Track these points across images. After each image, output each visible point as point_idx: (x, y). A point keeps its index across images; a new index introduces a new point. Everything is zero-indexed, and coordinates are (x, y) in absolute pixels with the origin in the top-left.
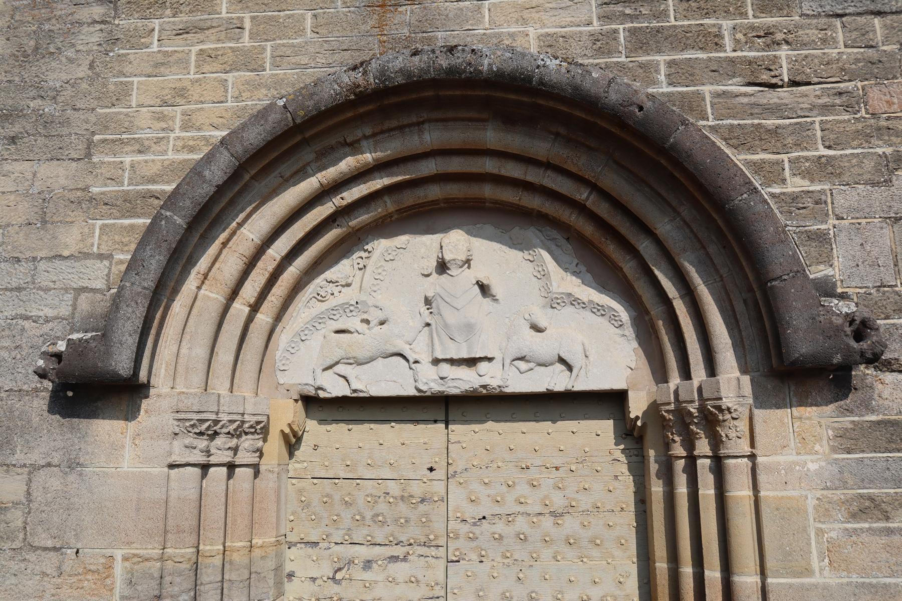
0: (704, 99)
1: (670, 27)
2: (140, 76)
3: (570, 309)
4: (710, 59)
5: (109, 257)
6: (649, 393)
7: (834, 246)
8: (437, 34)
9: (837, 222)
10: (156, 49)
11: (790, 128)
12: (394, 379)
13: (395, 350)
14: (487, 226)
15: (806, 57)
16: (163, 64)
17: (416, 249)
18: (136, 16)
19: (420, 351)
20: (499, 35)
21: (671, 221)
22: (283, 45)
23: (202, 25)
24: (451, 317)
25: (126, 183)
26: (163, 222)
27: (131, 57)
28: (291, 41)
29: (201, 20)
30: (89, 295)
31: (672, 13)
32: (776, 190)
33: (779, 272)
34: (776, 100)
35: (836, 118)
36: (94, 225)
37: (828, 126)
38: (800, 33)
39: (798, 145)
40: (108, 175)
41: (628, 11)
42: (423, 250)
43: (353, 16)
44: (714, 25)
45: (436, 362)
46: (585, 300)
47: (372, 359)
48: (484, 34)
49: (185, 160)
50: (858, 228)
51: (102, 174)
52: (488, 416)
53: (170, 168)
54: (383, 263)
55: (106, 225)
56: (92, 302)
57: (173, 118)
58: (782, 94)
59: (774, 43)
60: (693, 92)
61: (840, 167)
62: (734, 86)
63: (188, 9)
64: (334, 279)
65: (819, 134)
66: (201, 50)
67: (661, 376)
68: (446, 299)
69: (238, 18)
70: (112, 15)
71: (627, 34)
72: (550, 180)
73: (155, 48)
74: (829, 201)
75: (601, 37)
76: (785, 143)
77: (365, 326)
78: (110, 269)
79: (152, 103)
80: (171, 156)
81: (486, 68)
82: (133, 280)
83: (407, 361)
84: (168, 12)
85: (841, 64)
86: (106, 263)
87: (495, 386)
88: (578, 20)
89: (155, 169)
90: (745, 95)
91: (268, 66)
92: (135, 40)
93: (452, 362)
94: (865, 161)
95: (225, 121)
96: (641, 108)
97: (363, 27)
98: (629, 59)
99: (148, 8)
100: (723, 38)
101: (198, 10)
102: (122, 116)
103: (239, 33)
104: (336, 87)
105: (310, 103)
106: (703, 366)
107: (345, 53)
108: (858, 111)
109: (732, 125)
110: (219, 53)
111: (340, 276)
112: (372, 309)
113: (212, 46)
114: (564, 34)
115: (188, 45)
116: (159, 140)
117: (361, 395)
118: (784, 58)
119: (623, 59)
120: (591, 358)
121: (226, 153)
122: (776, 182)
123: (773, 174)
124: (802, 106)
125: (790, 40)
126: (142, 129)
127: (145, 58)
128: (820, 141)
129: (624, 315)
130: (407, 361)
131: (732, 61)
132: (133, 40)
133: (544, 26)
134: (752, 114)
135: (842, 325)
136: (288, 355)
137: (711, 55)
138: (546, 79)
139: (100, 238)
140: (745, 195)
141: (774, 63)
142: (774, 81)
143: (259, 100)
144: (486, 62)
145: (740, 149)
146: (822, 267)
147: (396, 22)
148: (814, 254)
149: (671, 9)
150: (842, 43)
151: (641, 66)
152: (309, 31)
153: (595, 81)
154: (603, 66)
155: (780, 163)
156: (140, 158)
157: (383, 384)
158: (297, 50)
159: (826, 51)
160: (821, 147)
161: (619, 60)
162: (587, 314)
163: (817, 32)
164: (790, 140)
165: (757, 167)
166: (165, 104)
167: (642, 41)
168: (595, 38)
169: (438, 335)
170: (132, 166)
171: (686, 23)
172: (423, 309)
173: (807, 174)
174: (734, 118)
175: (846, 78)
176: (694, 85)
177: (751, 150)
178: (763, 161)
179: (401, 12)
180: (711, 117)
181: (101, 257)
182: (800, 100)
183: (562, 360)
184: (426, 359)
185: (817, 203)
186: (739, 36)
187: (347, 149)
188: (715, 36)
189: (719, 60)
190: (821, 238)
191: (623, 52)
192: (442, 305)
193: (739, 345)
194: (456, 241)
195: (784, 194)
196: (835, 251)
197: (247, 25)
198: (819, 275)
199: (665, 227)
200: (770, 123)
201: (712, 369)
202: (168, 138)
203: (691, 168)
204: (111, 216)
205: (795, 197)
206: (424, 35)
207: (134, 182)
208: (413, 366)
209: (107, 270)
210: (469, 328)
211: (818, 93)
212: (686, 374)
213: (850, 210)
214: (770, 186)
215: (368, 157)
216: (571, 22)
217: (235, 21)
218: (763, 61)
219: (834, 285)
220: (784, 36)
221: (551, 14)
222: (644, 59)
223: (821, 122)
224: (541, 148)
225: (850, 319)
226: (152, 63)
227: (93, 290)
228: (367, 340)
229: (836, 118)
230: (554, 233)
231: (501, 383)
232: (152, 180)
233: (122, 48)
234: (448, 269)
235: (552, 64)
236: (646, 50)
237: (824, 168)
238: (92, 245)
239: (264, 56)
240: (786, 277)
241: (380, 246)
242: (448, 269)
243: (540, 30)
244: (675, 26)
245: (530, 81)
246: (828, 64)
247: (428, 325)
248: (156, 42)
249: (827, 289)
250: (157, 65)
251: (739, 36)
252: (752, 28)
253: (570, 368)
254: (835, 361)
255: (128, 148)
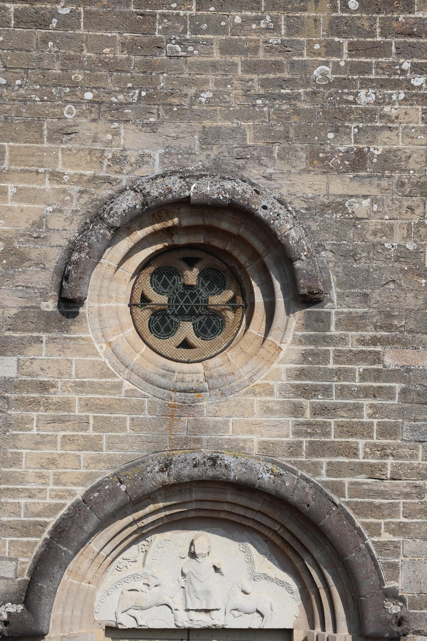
0: (344, 486)
1: (331, 442)
2: (27, 449)
3: (265, 581)
4: (350, 463)
5: (16, 560)
6: (305, 631)
7: (400, 571)
8: (202, 436)
9: (403, 558)
10: (36, 433)
11: (387, 506)
12: (163, 618)
13: (164, 603)
14: (219, 529)
15: (401, 464)
16: (41, 443)
17: (180, 538)
18: (22, 409)
19: (178, 603)
20: (237, 440)
21: (321, 551)
22: (114, 436)
23: (63, 419)
24: (198, 586)
25: (22, 515)
26: (63, 554)
27: (21, 436)
28: (118, 434)
29: (63, 415)
30: (5, 581)
31: (333, 433)
32: (376, 539)
33: (365, 593)
34: (382, 488)
35: (412, 501)
36: (5, 540)
37: (407, 506)
38: (400, 450)
39: (390, 515)
40: (12, 511)
41: (309, 430)
42: (181, 542)
43: (155, 421)
44: (355, 442)
45: (187, 610)
46: (273, 577)
47: (150, 607)
48: (229, 439)
49: (57, 504)
50: (413, 562)
51: (7, 510)
52: (213, 637)
53: (53, 509)
54: (157, 549)
55: (12, 541)
56: (7, 585)
57: (48, 477)
58: (387, 484)
59: (385, 455)
60: (339, 482)
61: (410, 529)
62: (361, 479)
63: (54, 407)
64: (128, 558)
65: (401, 509)
66: (64, 436)
67: (313, 627)
68: (195, 575)
69: (86, 416)
70: (6, 408)
71: (308, 444)
72: (259, 518)
73: (34, 431)
74: (401, 547)
75: (293, 445)
76: (384, 513)
77: (146, 587)
78: (16, 567)
79: (35, 467)
80: (49, 501)
81: (232, 477)
82: (48, 584)
83: (171, 608)
84: (42, 408)
85: (418, 470)
86: (14, 563)
87: (220, 625)
88: (282, 433)
89: (40, 508)
90: (367, 484)
91: (104, 448)
93: (197, 610)
94: (422, 526)
95: (79, 481)
96: (308, 506)
97: (160, 429)
98: (307, 459)
99: (29, 405)
100: (359, 450)
101: (61, 409)
102: (17, 474)
103: (87, 426)
104: (154, 483)
105: (140, 491)
106: (331, 625)
107: (150, 444)
108: (423, 498)
109: (357, 502)
110: (75, 438)
111: (131, 556)
112: (151, 578)
113: (71, 433)
114: (273, 442)
115: (55, 431)
116: (41, 491)
117: (144, 627)
118: (389, 465)
119: (304, 459)
120: (274, 611)
121: (95, 517)
123: (375, 530)
124: (396, 493)
125: (394, 454)
126: (30, 483)
127: (29, 438)
128: (401, 514)
129: (295, 587)
130: (171, 608)
131: (361, 464)
132: (21, 425)
133: (262, 436)
134: (368, 496)
135: (391, 620)
136: (100, 604)
137: (351, 460)
138: (263, 486)
139: (9, 548)
140: (354, 554)
141: (384, 467)
142: (383, 477)
143: (100, 469)
144: (232, 474)
145: (360, 515)
146: (393, 582)
147: (180, 427)
148: (390, 575)
149: (333, 430)
150: (420, 458)
151: (313, 464)
152: (128, 428)
153: (287, 489)
154: (293, 462)
155: (379, 525)
156: (30, 500)
157: (156, 622)
158: (122, 440)
159: (412, 462)
160: (401, 517)
161: (302, 459)
162: (274, 584)
163: (408, 450)
164: (386, 512)
165: (368, 526)
166: (43, 467)
167: (316, 449)
168: (290, 445)
169: (189, 595)
170: (26, 506)
171: (340, 440)
172: (180, 577)
173: (393, 532)
174: (359, 497)
175: (420, 478)
176: (340, 477)
177: (366, 516)
178: (371, 523)
179: (182, 421)
180: (347, 496)
181: (11, 559)
182: (395, 489)
183: (258, 611)
184: (181, 608)
185: (395, 547)
186: (368, 450)
187: (149, 500)
188: (354, 449)
189: (355, 464)
190: (394, 567)
191: (304, 455)
192: (193, 578)
193: (348, 618)
195: (379, 542)
196: (400, 574)
197: (91, 421)
198: (391, 586)
199: (317, 555)
200: (378, 501)
201: (335, 630)
202: (46, 489)
203: (330, 538)
204: (15, 536)
205: (385, 544)
206: (195, 437)
207: (28, 515)
208: (174, 612)
209: (15, 567)
210: (208, 593)
211: (405, 485)
212: (323, 628)
213: (412, 552)
214: (373, 537)
215: (161, 505)
216: (278, 435)
217: (84, 418)
218: (378, 465)
219: (398, 592)
220: (391, 451)
221: (267, 429)
222: (315, 460)
223: (404, 503)
225: (396, 615)
226: (34, 442)
227: (7, 579)
228: (148, 596)
229: (412, 501)
230: (258, 537)
231: (224, 624)
232: (38, 515)
233: (14, 430)
234: (197, 558)
235: (266, 476)
236: (317, 455)
237: (401, 529)
238: (5, 552)
239: (102, 442)
240: (368, 596)
241: (157, 538)
242: (197, 558)
243: (260, 439)
244: (334, 442)
245: (254, 486)
246: (412, 469)
247: (183, 587)
248: (35, 427)
250: (37, 443)
251: (368, 450)
252: (375, 445)
253: (262, 616)
254: (386, 636)
255: (22, 495)
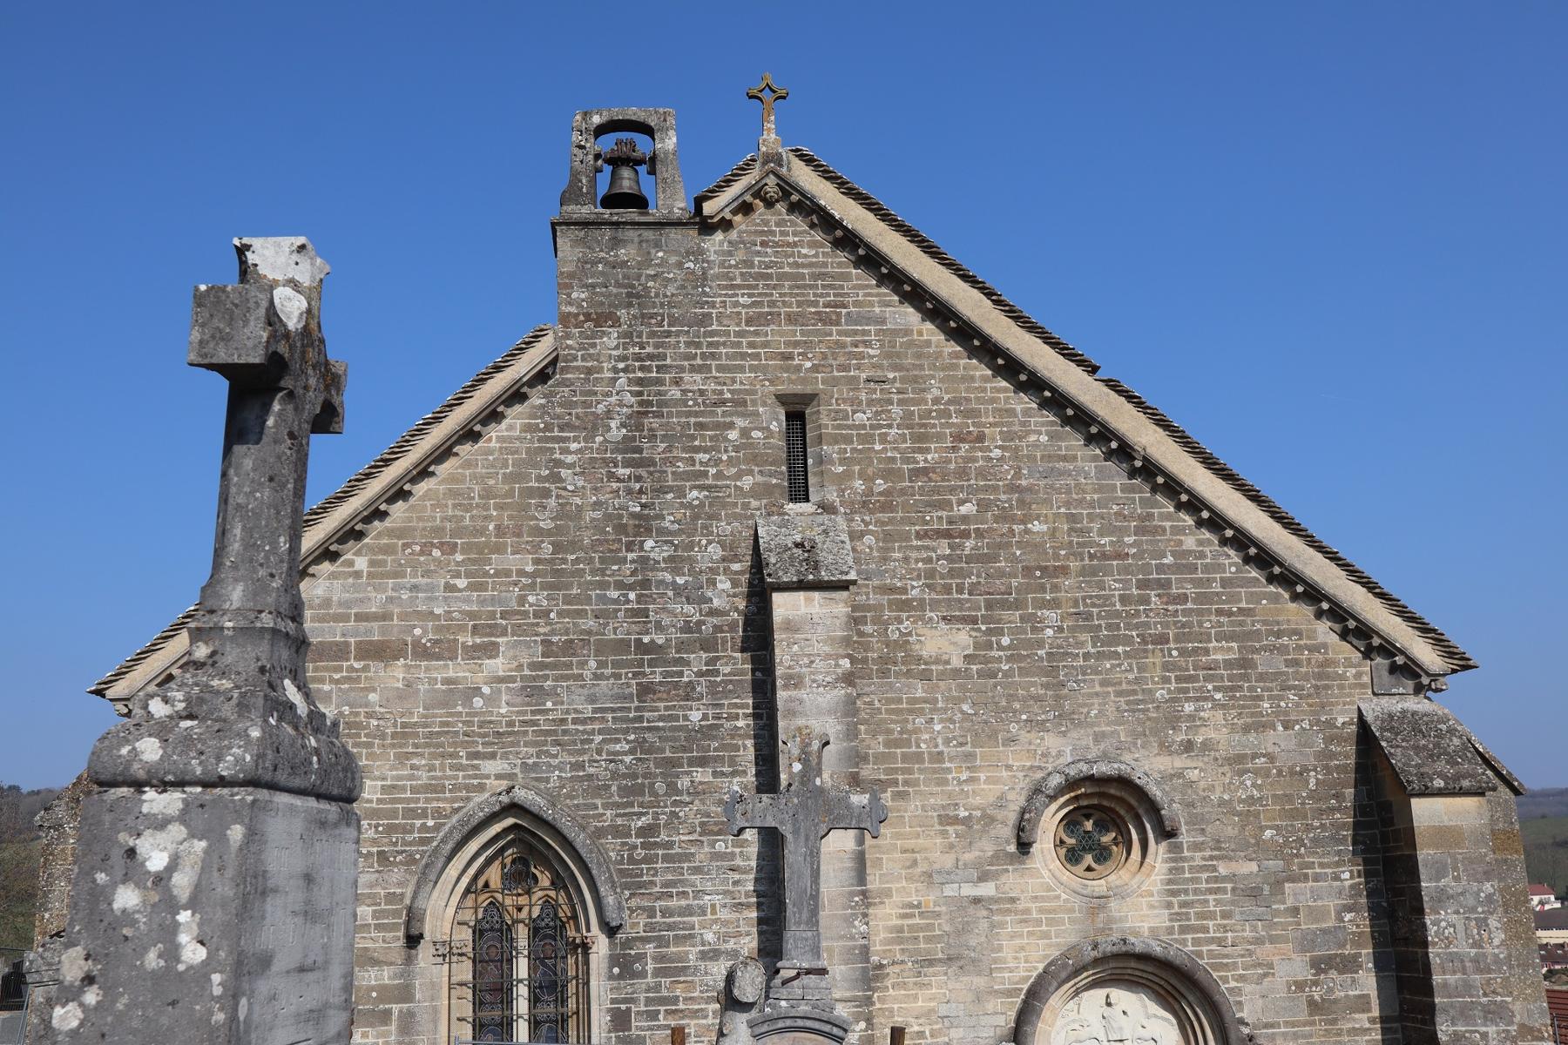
17: (1099, 994)
62: (1213, 947)
92: (1002, 925)
122: (1227, 984)
129: (1170, 1017)
165: (1221, 977)
190: (1240, 1003)
194: (1117, 994)
199: (1191, 998)
210: (1121, 1029)
224: (1150, 969)
235: (1154, 943)
237: (1241, 978)
249: (1242, 1022)
